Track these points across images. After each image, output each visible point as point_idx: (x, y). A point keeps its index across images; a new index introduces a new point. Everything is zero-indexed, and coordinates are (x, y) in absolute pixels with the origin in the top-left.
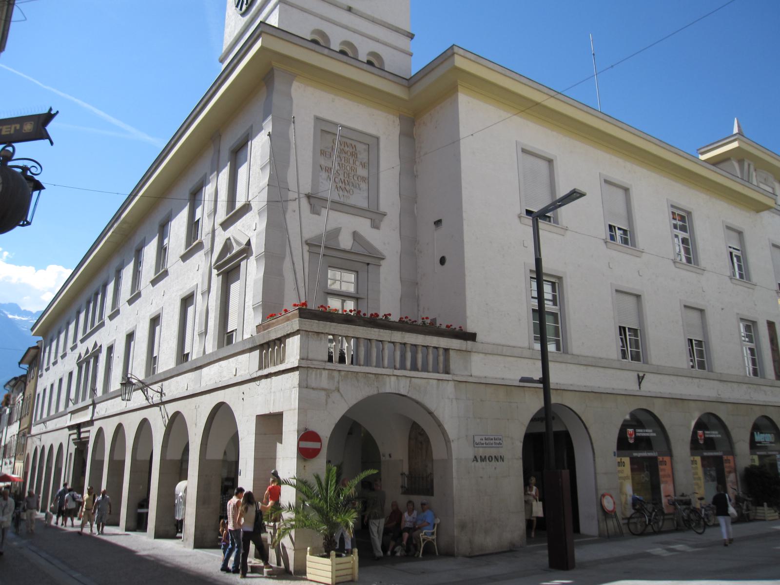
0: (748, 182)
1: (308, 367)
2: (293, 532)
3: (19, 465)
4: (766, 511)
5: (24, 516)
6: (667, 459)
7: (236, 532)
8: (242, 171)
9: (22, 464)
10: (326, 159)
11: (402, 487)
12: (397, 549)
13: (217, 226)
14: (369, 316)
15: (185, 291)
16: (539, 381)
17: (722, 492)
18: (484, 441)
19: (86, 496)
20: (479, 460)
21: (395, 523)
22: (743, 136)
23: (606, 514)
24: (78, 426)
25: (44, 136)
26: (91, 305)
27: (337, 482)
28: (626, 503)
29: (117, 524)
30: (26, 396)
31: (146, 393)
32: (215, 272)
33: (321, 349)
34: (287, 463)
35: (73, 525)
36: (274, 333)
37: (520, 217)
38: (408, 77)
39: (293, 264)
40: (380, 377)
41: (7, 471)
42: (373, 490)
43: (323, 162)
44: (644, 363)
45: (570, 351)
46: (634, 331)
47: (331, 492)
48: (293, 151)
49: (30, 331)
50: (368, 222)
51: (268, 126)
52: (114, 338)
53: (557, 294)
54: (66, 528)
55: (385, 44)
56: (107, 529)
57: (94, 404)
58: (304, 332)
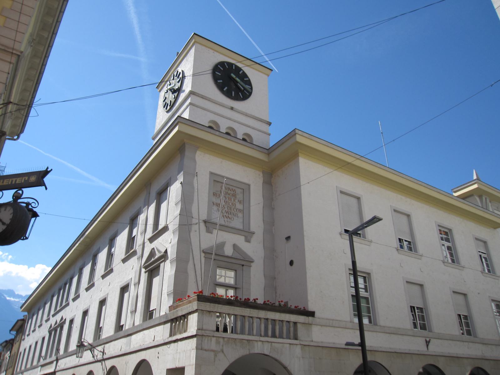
10: (217, 198)
13: (146, 240)
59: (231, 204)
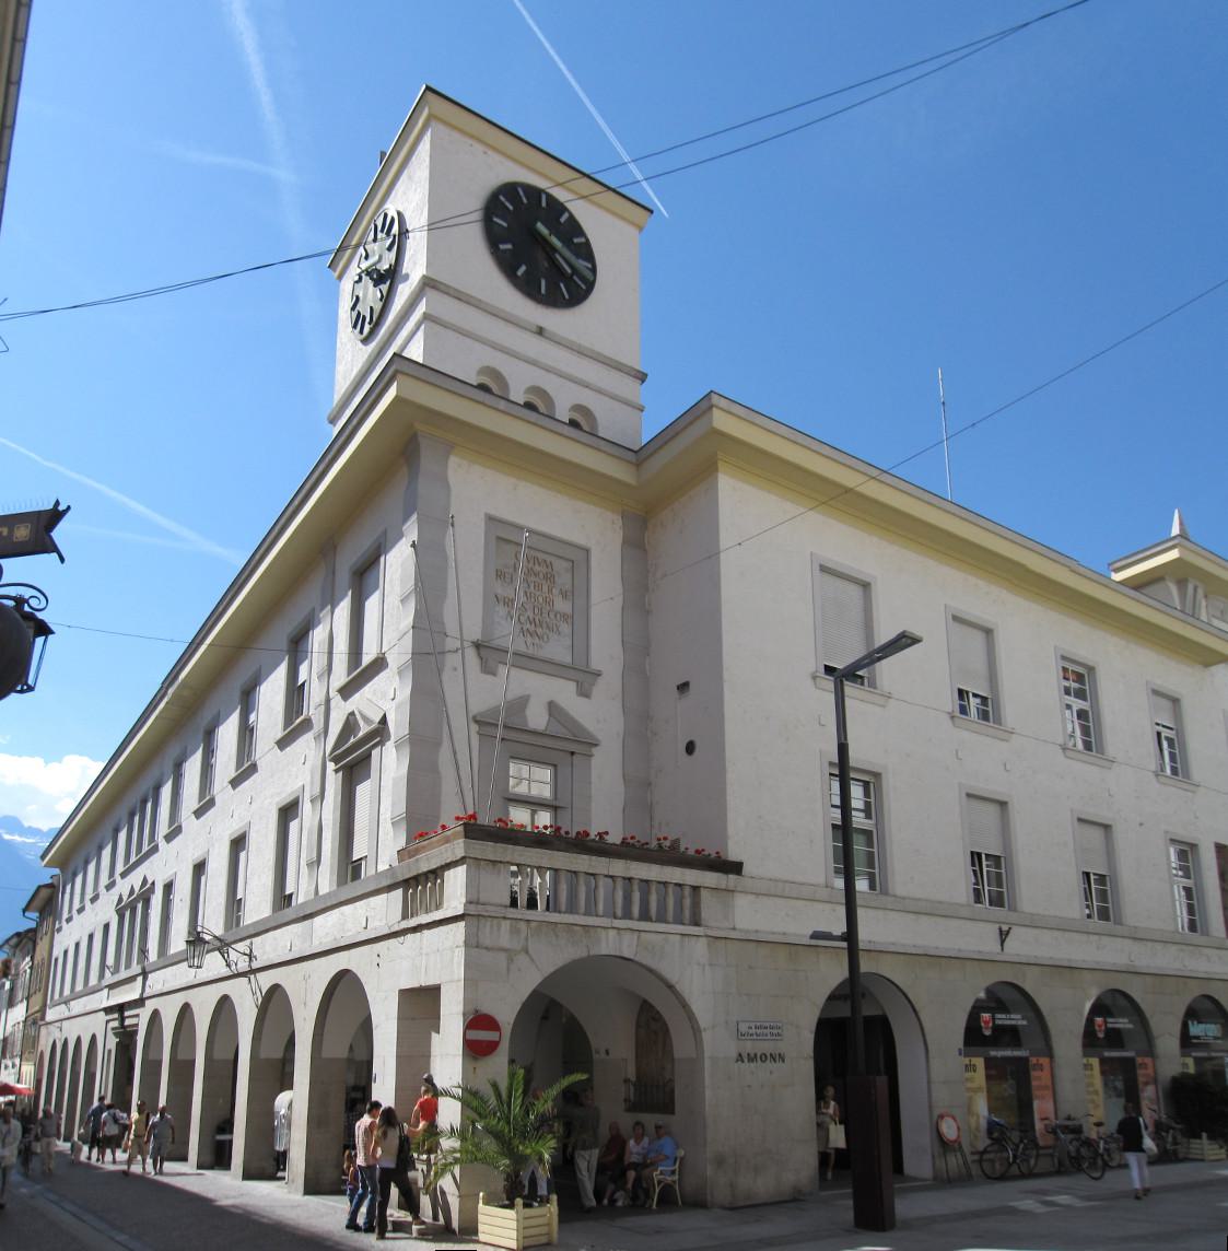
0: (1193, 616)
1: (479, 915)
2: (457, 1170)
3: (28, 1069)
4: (1207, 1147)
5: (38, 1148)
6: (1044, 1061)
7: (370, 1168)
8: (372, 605)
9: (33, 1067)
11: (625, 1100)
12: (617, 1195)
14: (574, 835)
15: (284, 795)
16: (842, 938)
17: (1134, 1115)
18: (753, 1031)
19: (135, 1115)
20: (746, 1060)
21: (613, 1157)
22: (1189, 540)
23: (944, 1145)
25: (48, 547)
26: (137, 819)
27: (525, 1093)
28: (977, 1129)
29: (184, 1158)
30: (36, 962)
31: (226, 955)
32: (331, 766)
33: (499, 888)
34: (447, 1064)
35: (115, 1160)
36: (425, 864)
37: (814, 678)
38: (636, 448)
39: (455, 753)
40: (592, 930)
41: (8, 1077)
42: (582, 1105)
43: (500, 589)
44: (1009, 909)
45: (890, 891)
46: (996, 860)
47: (515, 1108)
48: (452, 573)
49: (39, 860)
50: (572, 686)
51: (411, 532)
52: (175, 870)
53: (872, 800)
54: (103, 1166)
55: (600, 391)
56: (168, 1166)
57: (145, 974)
58: (471, 860)
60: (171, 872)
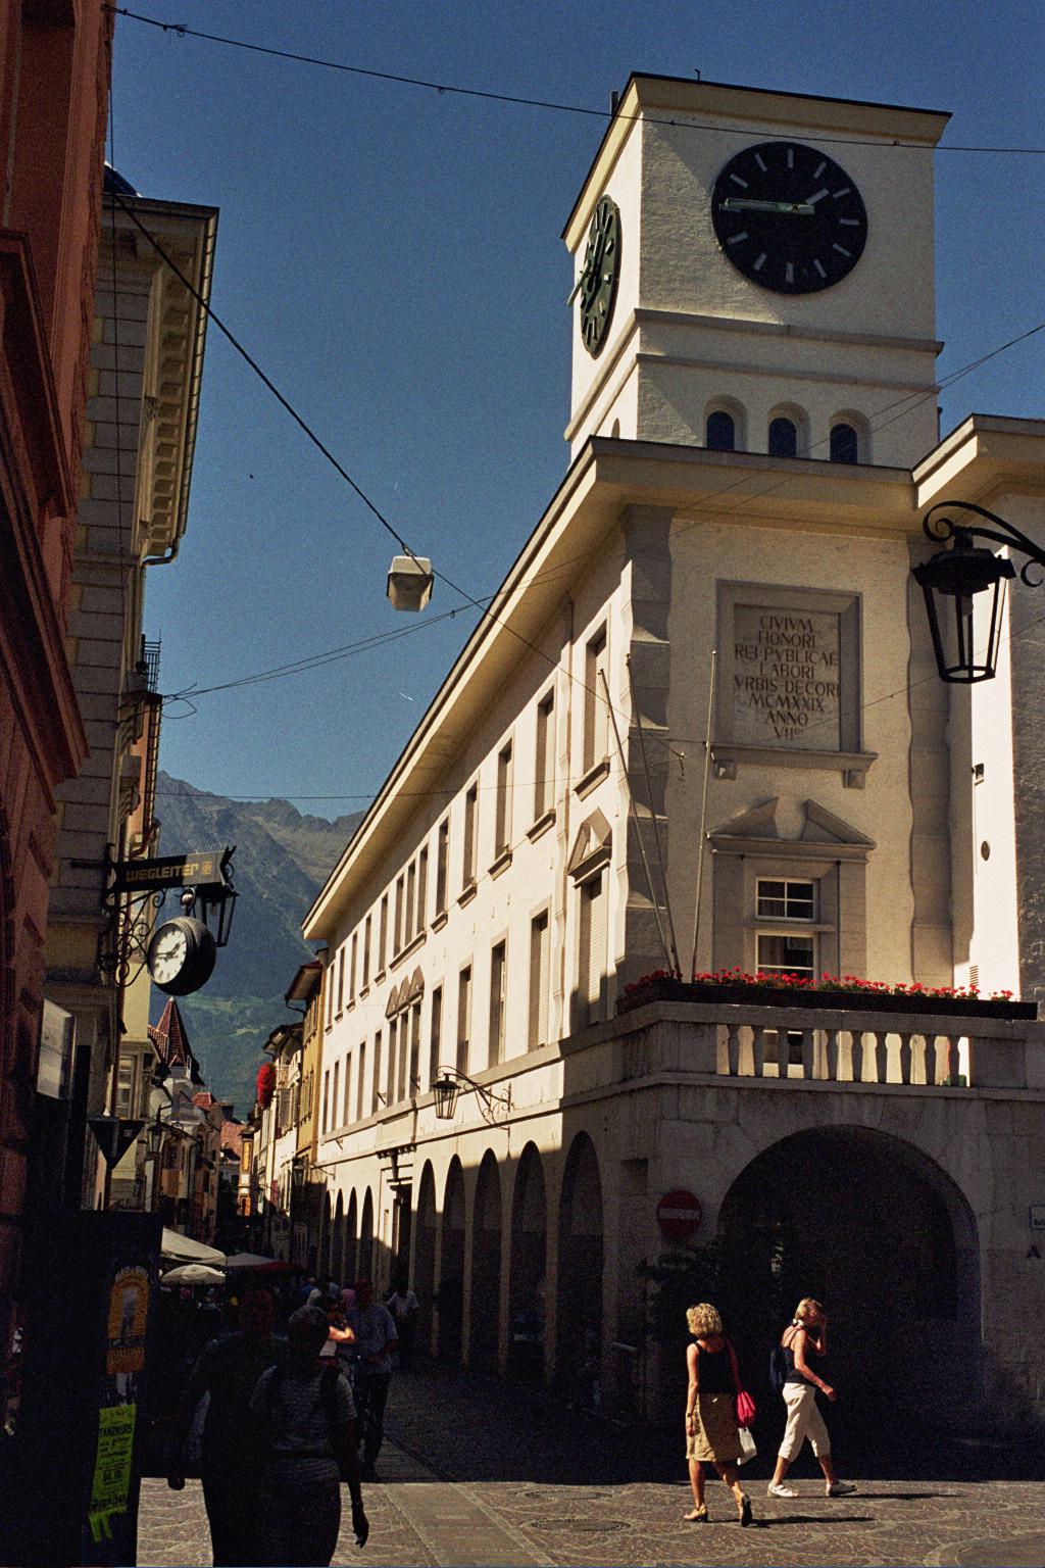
10: (748, 661)
13: (572, 792)
24: (394, 1153)
57: (415, 1109)
59: (796, 674)
60: (440, 977)
